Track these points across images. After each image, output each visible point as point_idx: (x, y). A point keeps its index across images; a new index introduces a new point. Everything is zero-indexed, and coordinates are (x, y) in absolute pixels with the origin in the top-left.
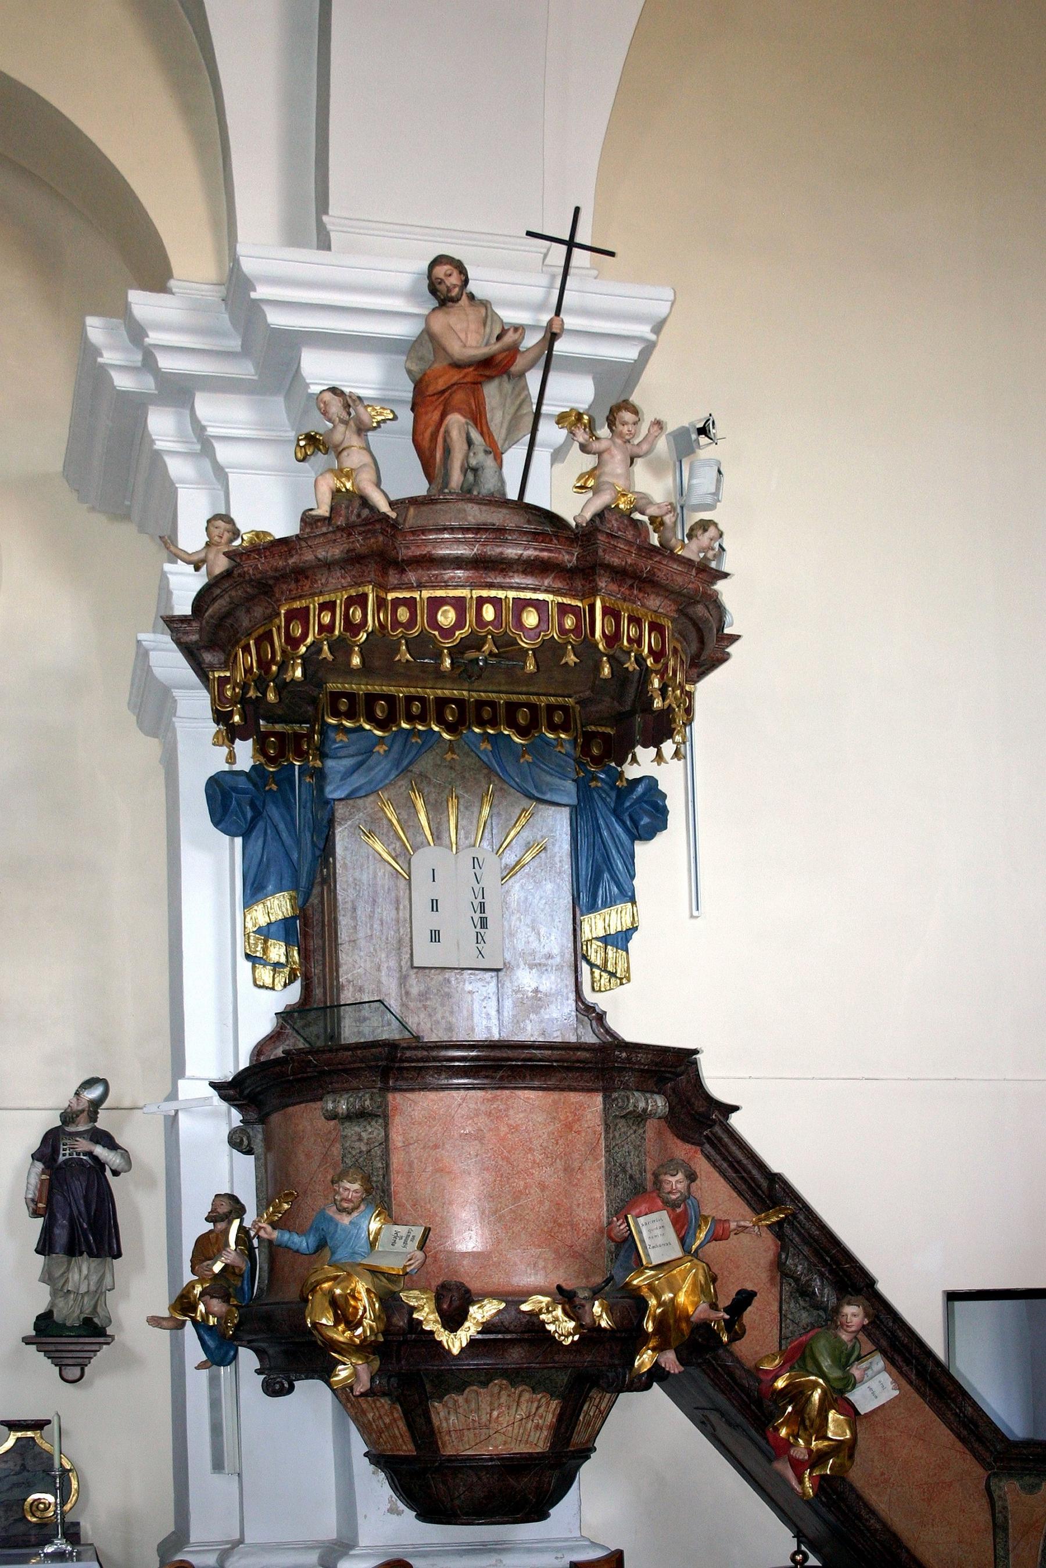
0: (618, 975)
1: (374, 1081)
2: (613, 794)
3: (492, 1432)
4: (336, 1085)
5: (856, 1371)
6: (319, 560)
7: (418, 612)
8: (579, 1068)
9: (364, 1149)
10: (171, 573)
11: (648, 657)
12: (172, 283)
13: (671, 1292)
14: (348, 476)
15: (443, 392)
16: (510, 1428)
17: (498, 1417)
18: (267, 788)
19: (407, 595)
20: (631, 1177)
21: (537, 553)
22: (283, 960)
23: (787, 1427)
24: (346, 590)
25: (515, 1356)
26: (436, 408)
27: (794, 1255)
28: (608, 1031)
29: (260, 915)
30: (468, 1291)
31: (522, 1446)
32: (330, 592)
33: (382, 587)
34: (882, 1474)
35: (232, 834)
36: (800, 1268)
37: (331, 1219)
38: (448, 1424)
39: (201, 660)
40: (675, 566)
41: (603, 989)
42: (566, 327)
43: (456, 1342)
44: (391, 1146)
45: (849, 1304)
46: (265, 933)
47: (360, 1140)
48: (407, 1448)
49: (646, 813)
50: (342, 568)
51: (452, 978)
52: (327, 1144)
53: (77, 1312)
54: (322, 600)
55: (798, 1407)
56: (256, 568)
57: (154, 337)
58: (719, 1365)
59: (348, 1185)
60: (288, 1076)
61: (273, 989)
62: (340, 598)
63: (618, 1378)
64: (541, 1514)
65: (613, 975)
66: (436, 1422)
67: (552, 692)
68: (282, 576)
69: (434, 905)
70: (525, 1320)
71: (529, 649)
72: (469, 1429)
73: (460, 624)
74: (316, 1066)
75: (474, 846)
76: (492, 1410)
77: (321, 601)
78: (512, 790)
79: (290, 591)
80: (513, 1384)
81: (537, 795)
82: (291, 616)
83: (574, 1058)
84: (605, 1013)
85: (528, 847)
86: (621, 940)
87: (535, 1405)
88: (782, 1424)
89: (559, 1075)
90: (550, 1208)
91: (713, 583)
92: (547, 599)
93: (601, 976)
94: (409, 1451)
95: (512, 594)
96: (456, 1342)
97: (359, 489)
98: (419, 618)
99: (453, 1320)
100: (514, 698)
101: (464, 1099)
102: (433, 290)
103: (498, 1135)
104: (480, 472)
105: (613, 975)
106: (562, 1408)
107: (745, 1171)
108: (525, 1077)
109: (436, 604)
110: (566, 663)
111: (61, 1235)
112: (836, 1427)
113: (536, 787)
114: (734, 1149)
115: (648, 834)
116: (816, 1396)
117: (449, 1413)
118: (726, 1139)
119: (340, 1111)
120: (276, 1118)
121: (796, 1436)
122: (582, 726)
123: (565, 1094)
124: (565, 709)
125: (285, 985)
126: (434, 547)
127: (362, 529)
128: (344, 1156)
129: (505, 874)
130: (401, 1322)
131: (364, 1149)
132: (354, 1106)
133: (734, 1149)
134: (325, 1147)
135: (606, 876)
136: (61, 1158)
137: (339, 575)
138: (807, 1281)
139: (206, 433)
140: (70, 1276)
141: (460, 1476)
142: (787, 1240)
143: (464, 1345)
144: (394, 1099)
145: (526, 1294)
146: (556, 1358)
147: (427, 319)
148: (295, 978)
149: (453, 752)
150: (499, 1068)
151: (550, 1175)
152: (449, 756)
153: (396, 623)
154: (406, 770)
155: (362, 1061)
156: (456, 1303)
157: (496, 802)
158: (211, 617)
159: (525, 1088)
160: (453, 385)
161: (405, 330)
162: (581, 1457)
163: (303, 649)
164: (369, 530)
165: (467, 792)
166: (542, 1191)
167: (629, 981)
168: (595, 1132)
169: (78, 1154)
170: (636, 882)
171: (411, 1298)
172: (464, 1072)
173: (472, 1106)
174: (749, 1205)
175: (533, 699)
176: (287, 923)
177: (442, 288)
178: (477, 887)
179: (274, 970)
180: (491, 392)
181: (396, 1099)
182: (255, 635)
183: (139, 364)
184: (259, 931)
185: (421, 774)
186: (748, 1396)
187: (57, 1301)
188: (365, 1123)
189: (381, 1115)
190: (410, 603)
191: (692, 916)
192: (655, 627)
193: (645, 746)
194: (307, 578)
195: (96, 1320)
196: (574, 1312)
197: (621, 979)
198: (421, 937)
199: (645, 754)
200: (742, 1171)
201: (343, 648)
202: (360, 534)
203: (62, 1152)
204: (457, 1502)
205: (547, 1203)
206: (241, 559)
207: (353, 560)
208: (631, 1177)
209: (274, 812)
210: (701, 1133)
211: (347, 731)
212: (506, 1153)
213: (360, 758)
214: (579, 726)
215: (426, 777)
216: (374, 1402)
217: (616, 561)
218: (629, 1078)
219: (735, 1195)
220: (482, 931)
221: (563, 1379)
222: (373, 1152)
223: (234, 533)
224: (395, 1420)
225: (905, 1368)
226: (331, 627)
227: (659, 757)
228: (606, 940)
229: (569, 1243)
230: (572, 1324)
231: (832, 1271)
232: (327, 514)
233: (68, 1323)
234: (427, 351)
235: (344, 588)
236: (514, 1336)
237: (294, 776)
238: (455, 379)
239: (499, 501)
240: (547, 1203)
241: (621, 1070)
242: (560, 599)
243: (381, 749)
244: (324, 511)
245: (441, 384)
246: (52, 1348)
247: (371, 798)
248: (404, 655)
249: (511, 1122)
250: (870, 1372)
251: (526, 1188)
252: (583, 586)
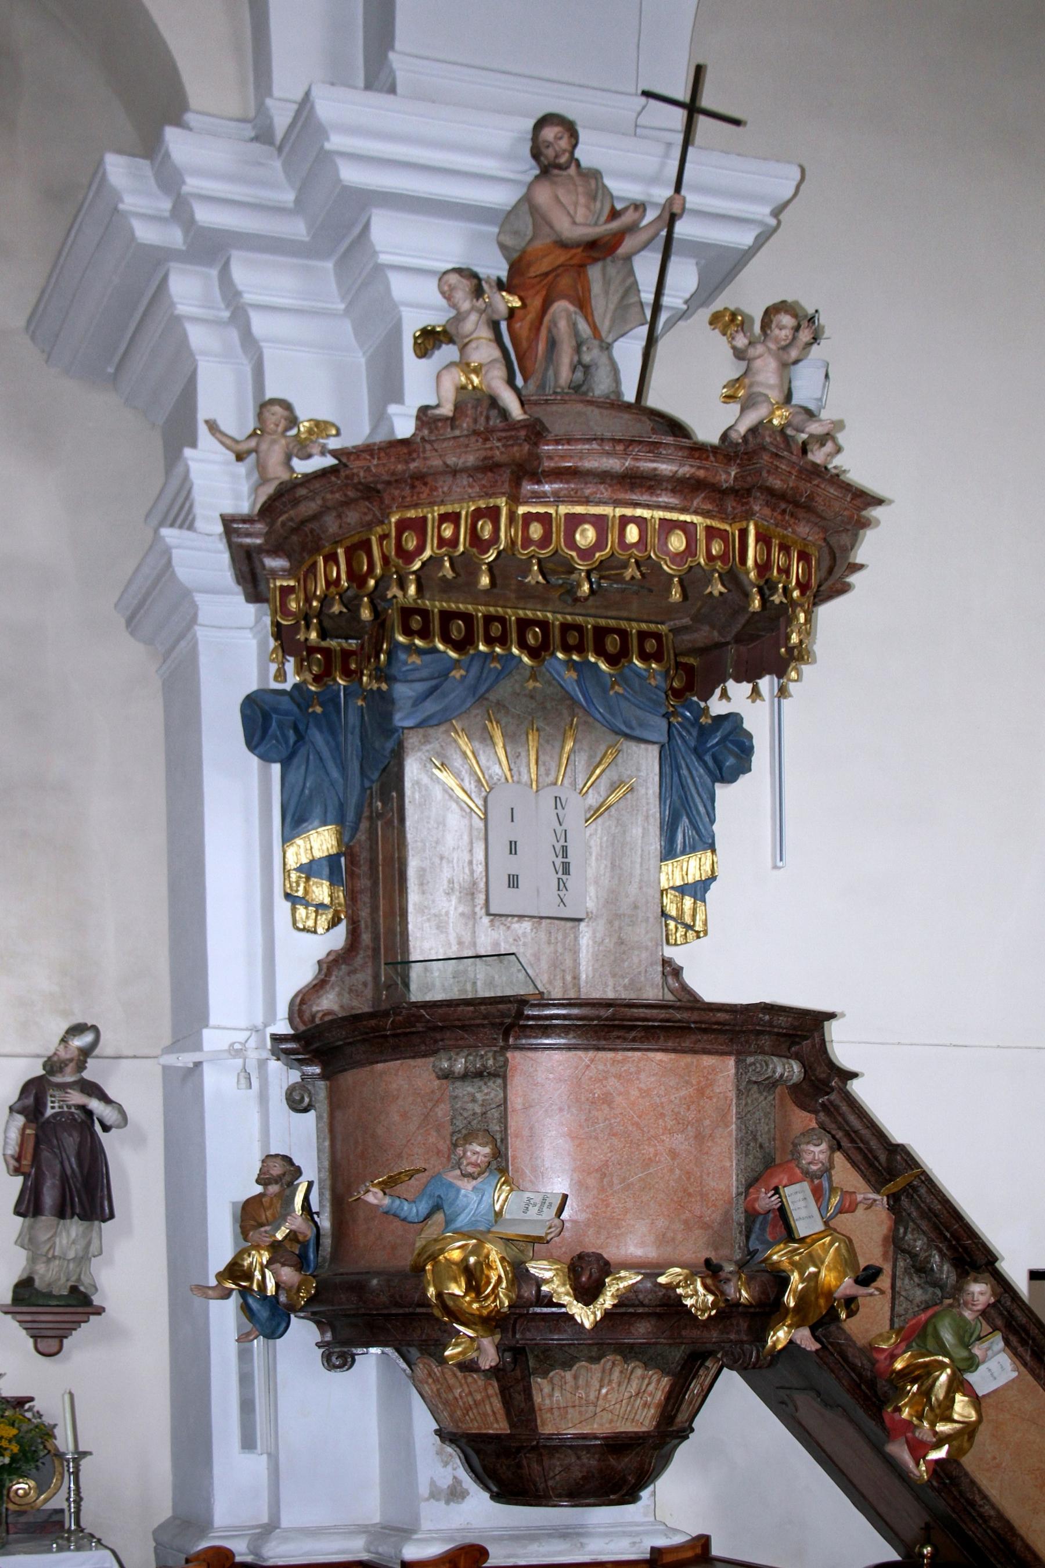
0: (697, 928)
1: (495, 1039)
2: (695, 733)
3: (598, 1410)
4: (448, 1042)
5: (977, 1350)
6: (448, 466)
7: (554, 529)
8: (715, 1030)
9: (478, 1110)
10: (193, 460)
11: (794, 589)
12: (190, 117)
13: (816, 1266)
14: (477, 371)
15: (546, 274)
16: (618, 1406)
17: (607, 1393)
18: (310, 710)
19: (541, 510)
20: (761, 1146)
21: (693, 470)
22: (327, 901)
23: (911, 1408)
24: (473, 501)
25: (641, 1331)
26: (538, 293)
27: (913, 1230)
28: (685, 988)
29: (299, 853)
30: (607, 1263)
31: (628, 1424)
32: (453, 503)
33: (515, 499)
34: (994, 1458)
35: (266, 758)
36: (919, 1243)
37: (451, 1185)
38: (552, 1402)
40: (832, 491)
41: (679, 942)
42: (688, 206)
43: (586, 1316)
44: (509, 1110)
45: (976, 1281)
46: (309, 870)
47: (474, 1100)
48: (500, 1426)
49: (731, 752)
50: (470, 476)
52: (430, 1105)
53: (63, 1280)
54: (443, 510)
55: (924, 1388)
56: (368, 469)
57: (192, 184)
58: (831, 1344)
59: (478, 1149)
60: (385, 1030)
61: (315, 932)
62: (466, 509)
63: (745, 1355)
64: (630, 1496)
65: (689, 927)
66: (537, 1399)
67: (645, 617)
68: (397, 481)
69: (513, 848)
70: (660, 1294)
71: (675, 576)
72: (574, 1407)
73: (600, 543)
74: (428, 1021)
75: (555, 784)
76: (601, 1387)
77: (442, 512)
78: (598, 725)
79: (404, 497)
80: (626, 1359)
81: (628, 731)
82: (403, 526)
83: (713, 1020)
84: (682, 968)
85: (614, 788)
86: (698, 890)
87: (646, 1381)
88: (905, 1405)
89: (693, 1038)
90: (680, 1177)
91: (864, 509)
92: (695, 521)
93: (677, 928)
94: (501, 1429)
95: (660, 514)
96: (586, 1316)
97: (489, 386)
98: (554, 536)
99: (588, 1294)
100: (602, 622)
101: (592, 1061)
102: (536, 154)
103: (628, 1099)
104: (593, 369)
105: (689, 927)
106: (671, 1386)
107: (862, 1141)
108: (659, 1038)
109: (574, 521)
110: (711, 593)
111: (49, 1198)
112: (962, 1408)
113: (625, 723)
114: (852, 1118)
115: (728, 778)
116: (943, 1378)
117: (553, 1389)
118: (844, 1108)
119: (457, 1071)
120: (349, 1078)
121: (921, 1417)
122: (676, 655)
123: (698, 1057)
124: (657, 636)
125: (328, 930)
126: (581, 458)
127: (504, 434)
128: (453, 1118)
129: (588, 816)
130: (529, 1292)
131: (478, 1110)
132: (474, 1066)
133: (852, 1118)
134: (426, 1107)
135: (685, 820)
136: (49, 1112)
137: (465, 482)
138: (926, 1257)
139: (242, 301)
140: (57, 1240)
141: (557, 1455)
142: (904, 1214)
143: (598, 1319)
144: (514, 1058)
145: (660, 1268)
146: (684, 1333)
147: (531, 186)
148: (340, 920)
149: (536, 680)
150: (633, 1028)
151: (680, 1142)
152: (531, 684)
153: (527, 541)
154: (482, 697)
155: (485, 1017)
156: (595, 1275)
157: (579, 736)
158: (291, 519)
159: (657, 1050)
160: (559, 266)
161: (503, 197)
162: (680, 1437)
163: (417, 565)
164: (511, 437)
165: (548, 724)
166: (673, 1159)
167: (706, 934)
168: (726, 1098)
169: (69, 1107)
170: (715, 827)
171: (541, 1269)
172: (565, 1030)
173: (601, 1067)
174: (864, 1176)
175: (624, 624)
176: (332, 860)
177: (550, 153)
178: (559, 830)
179: (316, 912)
180: (594, 272)
181: (515, 1058)
182: (348, 543)
183: (167, 214)
184: (300, 869)
185: (498, 703)
186: (860, 1375)
187: (38, 1267)
188: (481, 1083)
189: (500, 1074)
190: (545, 519)
191: (775, 867)
192: (803, 556)
193: (738, 680)
194: (425, 484)
195: (82, 1289)
196: (717, 1288)
197: (698, 932)
198: (498, 883)
199: (739, 690)
200: (859, 1141)
201: (465, 567)
202: (499, 440)
203: (50, 1104)
204: (550, 1483)
205: (677, 1172)
206: (348, 459)
207: (489, 467)
208: (761, 1146)
209: (317, 738)
210: (817, 1101)
211: (420, 651)
212: (636, 1119)
213: (433, 682)
214: (672, 656)
215: (504, 706)
216: (465, 1378)
217: (777, 483)
218: (766, 1041)
219: (849, 1165)
220: (564, 877)
221: (677, 1355)
222: (489, 1115)
223: (291, 422)
224: (488, 1397)
225: (1020, 1349)
226: (454, 542)
227: (756, 693)
228: (682, 890)
229: (698, 1214)
230: (710, 1298)
231: (951, 1247)
232: (451, 414)
233: (55, 1292)
234: (526, 224)
235: (471, 499)
236: (646, 1310)
237: (339, 697)
238: (562, 260)
239: (615, 404)
240: (677, 1172)
241: (759, 1033)
242: (709, 522)
243: (457, 674)
244: (447, 410)
245: (544, 266)
246: (28, 1318)
247: (442, 728)
248: (535, 577)
249: (642, 1086)
250: (990, 1353)
251: (656, 1155)
252: (733, 508)
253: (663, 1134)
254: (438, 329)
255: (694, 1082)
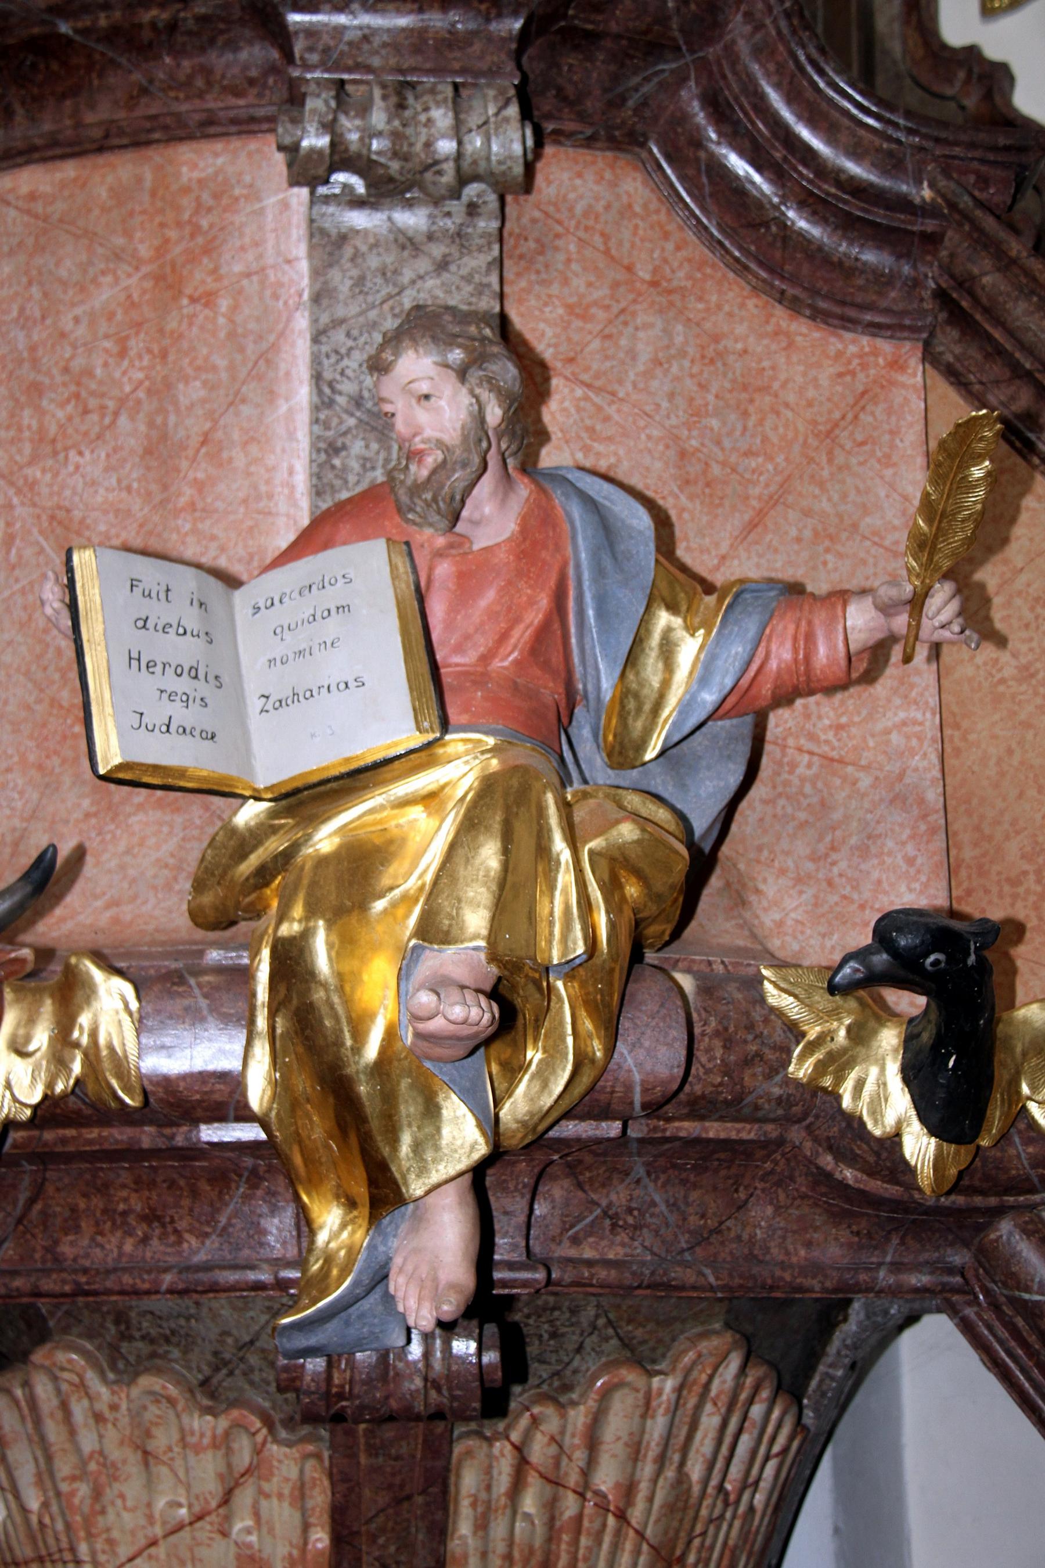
39: (721, 18)
51: (596, 1095)
123: (156, 155)
253: (33, 460)
254: (808, 312)
255: (144, 251)
